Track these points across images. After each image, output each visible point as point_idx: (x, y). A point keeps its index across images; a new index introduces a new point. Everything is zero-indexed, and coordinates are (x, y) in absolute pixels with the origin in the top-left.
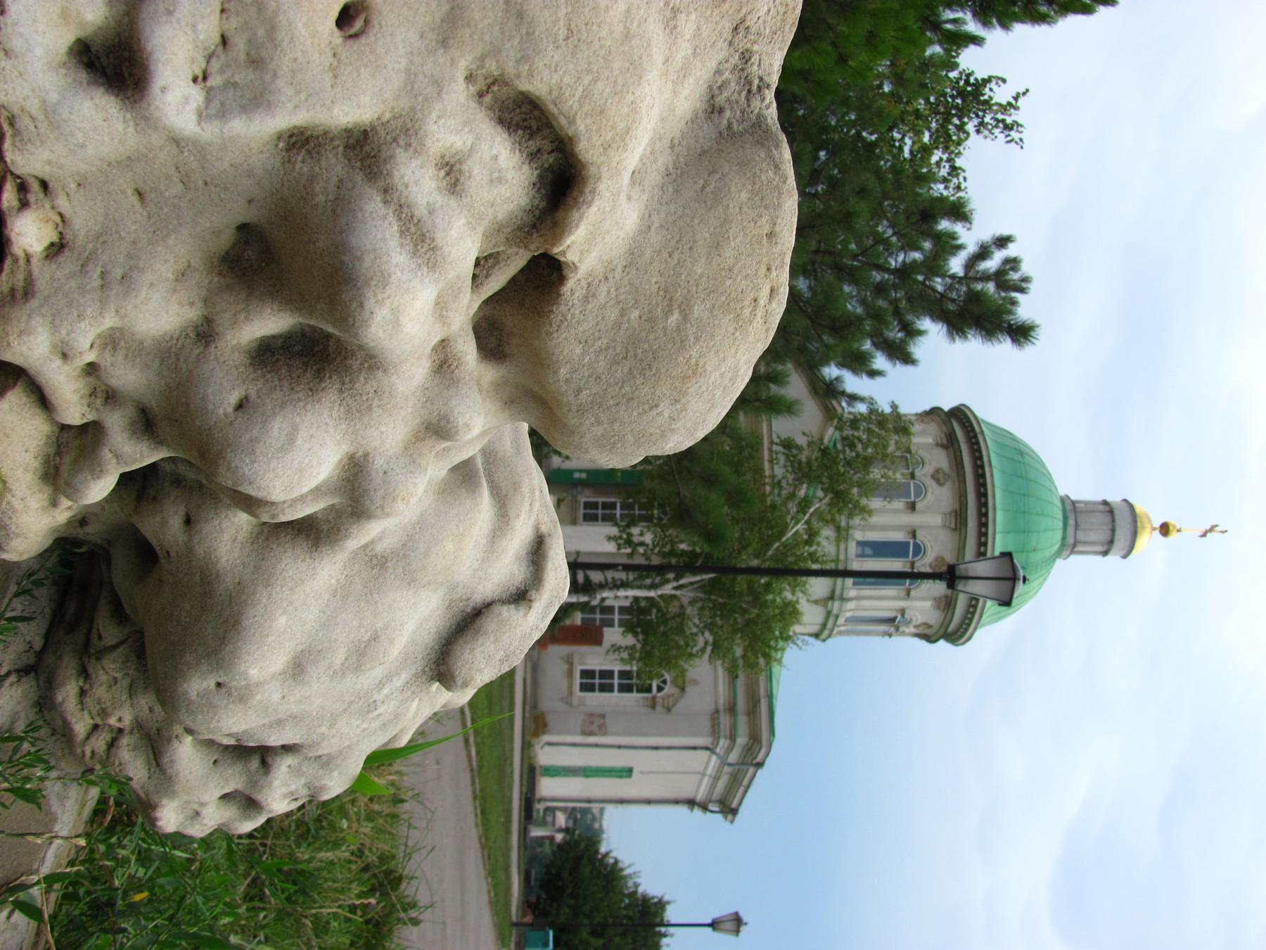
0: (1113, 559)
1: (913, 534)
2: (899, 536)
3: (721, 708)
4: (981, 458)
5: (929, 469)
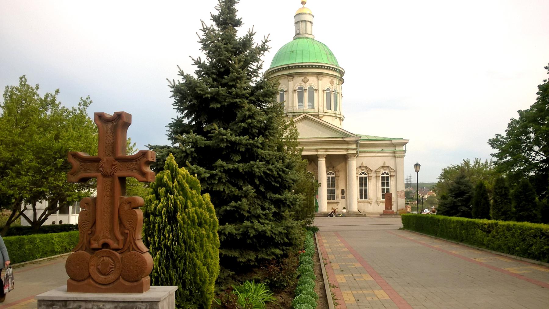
1: (295, 90)
2: (296, 95)
3: (393, 155)
4: (299, 66)
5: (303, 84)
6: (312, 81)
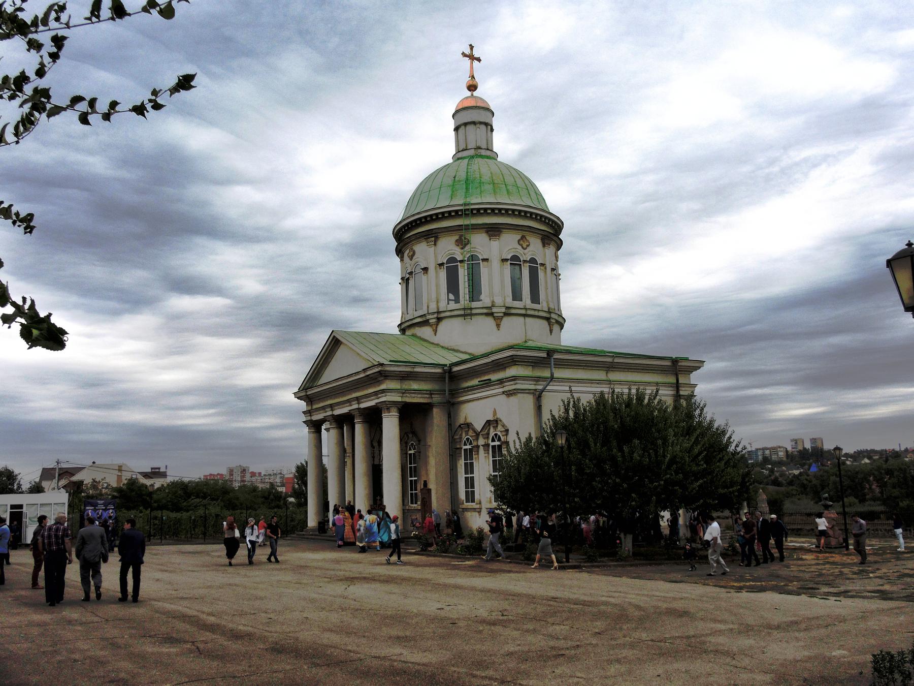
0: (495, 123)
2: (443, 274)
6: (480, 243)
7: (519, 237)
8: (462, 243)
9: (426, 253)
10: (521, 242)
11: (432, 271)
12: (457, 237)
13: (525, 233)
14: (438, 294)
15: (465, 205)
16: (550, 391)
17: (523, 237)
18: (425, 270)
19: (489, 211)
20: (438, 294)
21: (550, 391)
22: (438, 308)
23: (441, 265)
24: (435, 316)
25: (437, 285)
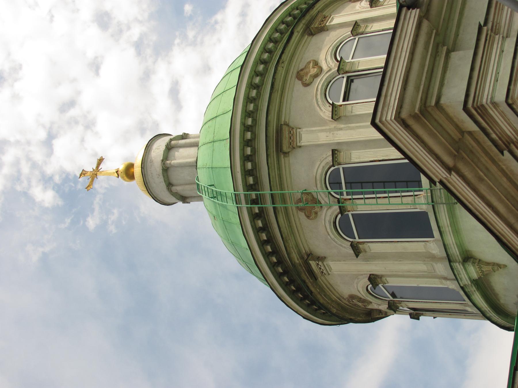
2: (376, 246)
6: (306, 172)
7: (298, 84)
8: (310, 205)
9: (344, 273)
10: (307, 78)
11: (376, 268)
12: (302, 215)
13: (293, 71)
14: (416, 256)
15: (237, 201)
16: (390, 29)
17: (299, 76)
18: (374, 280)
19: (248, 151)
20: (416, 256)
21: (390, 29)
22: (440, 259)
23: (356, 250)
24: (459, 267)
25: (400, 257)
